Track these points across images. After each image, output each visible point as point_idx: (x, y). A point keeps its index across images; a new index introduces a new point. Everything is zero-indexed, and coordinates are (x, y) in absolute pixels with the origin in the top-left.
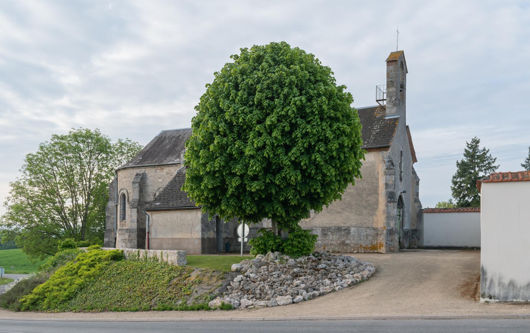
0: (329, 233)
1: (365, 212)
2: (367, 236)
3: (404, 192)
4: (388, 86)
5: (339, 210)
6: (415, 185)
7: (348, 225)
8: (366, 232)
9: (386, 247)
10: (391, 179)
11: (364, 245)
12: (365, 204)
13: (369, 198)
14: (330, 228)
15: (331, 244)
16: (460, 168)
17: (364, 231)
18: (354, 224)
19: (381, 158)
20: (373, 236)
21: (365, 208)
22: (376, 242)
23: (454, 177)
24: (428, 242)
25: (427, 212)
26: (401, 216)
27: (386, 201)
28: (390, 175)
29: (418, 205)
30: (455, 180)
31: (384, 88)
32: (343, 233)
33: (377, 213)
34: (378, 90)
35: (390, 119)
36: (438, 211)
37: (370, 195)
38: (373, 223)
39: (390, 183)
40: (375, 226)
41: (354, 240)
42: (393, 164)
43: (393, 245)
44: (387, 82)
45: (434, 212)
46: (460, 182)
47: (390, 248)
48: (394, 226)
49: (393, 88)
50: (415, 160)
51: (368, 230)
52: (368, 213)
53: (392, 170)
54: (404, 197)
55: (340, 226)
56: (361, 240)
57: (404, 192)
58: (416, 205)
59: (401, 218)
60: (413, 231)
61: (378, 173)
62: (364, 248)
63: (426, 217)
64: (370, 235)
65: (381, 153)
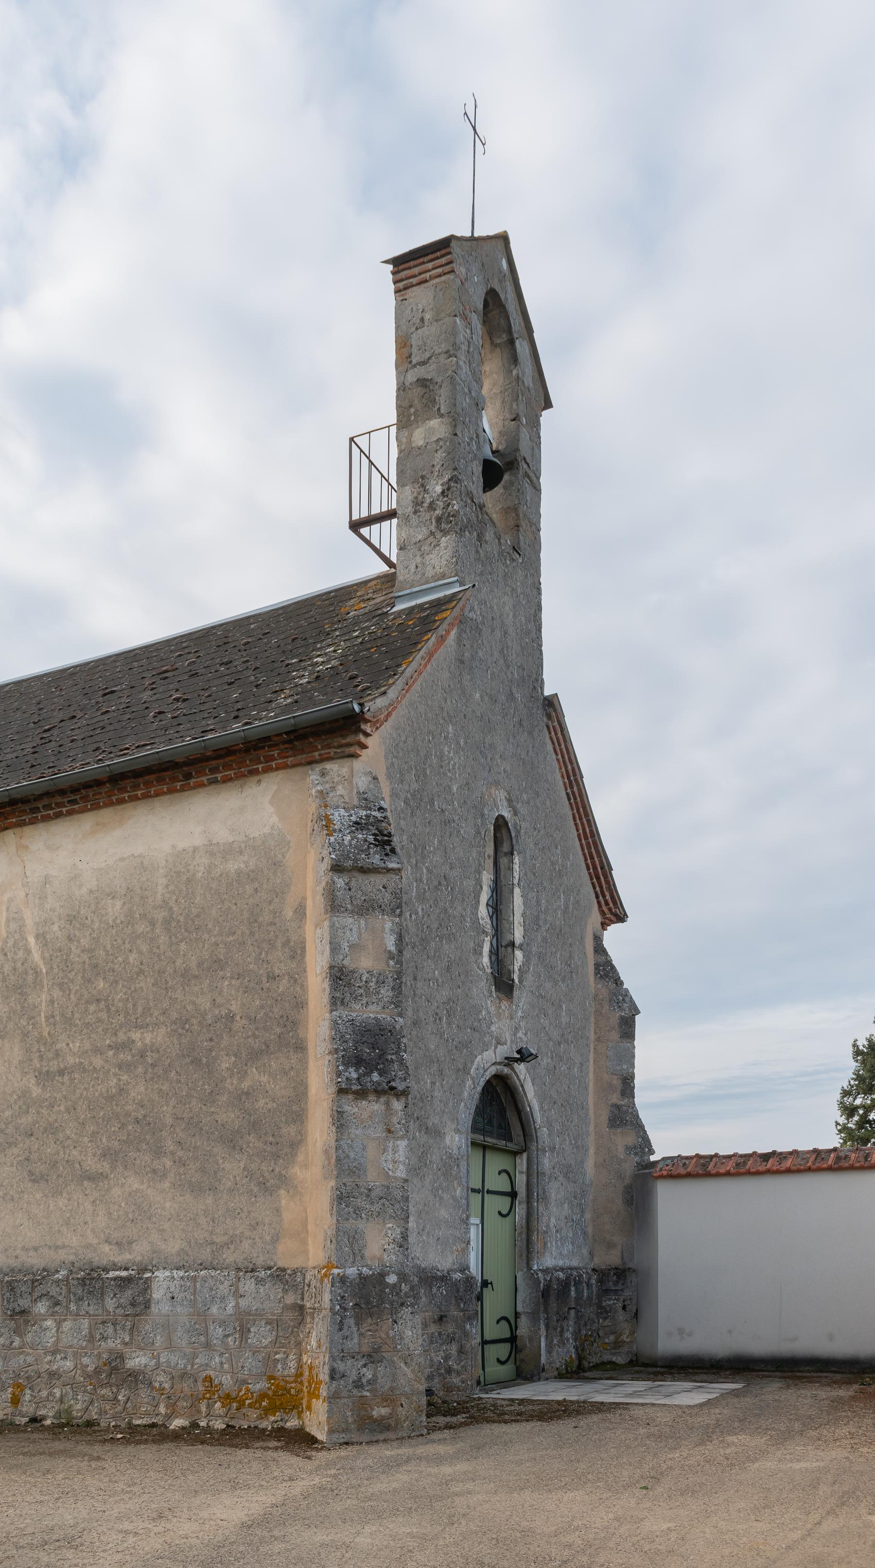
0: (41, 1308)
1: (232, 1167)
2: (243, 1324)
3: (524, 1056)
4: (407, 416)
5: (92, 1164)
6: (615, 1035)
7: (138, 1253)
8: (238, 1295)
9: (333, 1398)
10: (373, 943)
11: (227, 1381)
12: (230, 1117)
13: (255, 1076)
14: (48, 1272)
15: (53, 1375)
16: (863, 1062)
17: (224, 1289)
18: (173, 1247)
19: (313, 807)
20: (275, 1324)
21: (231, 1141)
22: (293, 1364)
23: (846, 1093)
24: (681, 1331)
25: (671, 1176)
26: (522, 1200)
27: (333, 1089)
28: (366, 908)
29: (631, 1139)
30: (848, 1100)
31: (385, 452)
32: (110, 1303)
33: (296, 1171)
34: (356, 451)
35: (411, 610)
36: (730, 1166)
37: (255, 1055)
38: (275, 1239)
39: (366, 963)
40: (286, 1256)
41: (170, 1347)
42: (384, 842)
43: (384, 1384)
44: (402, 389)
45: (708, 1175)
46: (863, 1106)
47: (362, 1404)
48: (391, 1258)
49: (434, 423)
50: (614, 912)
51: (248, 1285)
52: (249, 1174)
53: (378, 880)
54: (530, 1093)
55: (96, 1261)
56: (208, 1345)
57: (524, 1056)
58: (623, 1140)
59: (520, 1210)
60: (602, 1274)
61: (300, 911)
62: (227, 1398)
63: (670, 1201)
64: (259, 1314)
65: (313, 775)
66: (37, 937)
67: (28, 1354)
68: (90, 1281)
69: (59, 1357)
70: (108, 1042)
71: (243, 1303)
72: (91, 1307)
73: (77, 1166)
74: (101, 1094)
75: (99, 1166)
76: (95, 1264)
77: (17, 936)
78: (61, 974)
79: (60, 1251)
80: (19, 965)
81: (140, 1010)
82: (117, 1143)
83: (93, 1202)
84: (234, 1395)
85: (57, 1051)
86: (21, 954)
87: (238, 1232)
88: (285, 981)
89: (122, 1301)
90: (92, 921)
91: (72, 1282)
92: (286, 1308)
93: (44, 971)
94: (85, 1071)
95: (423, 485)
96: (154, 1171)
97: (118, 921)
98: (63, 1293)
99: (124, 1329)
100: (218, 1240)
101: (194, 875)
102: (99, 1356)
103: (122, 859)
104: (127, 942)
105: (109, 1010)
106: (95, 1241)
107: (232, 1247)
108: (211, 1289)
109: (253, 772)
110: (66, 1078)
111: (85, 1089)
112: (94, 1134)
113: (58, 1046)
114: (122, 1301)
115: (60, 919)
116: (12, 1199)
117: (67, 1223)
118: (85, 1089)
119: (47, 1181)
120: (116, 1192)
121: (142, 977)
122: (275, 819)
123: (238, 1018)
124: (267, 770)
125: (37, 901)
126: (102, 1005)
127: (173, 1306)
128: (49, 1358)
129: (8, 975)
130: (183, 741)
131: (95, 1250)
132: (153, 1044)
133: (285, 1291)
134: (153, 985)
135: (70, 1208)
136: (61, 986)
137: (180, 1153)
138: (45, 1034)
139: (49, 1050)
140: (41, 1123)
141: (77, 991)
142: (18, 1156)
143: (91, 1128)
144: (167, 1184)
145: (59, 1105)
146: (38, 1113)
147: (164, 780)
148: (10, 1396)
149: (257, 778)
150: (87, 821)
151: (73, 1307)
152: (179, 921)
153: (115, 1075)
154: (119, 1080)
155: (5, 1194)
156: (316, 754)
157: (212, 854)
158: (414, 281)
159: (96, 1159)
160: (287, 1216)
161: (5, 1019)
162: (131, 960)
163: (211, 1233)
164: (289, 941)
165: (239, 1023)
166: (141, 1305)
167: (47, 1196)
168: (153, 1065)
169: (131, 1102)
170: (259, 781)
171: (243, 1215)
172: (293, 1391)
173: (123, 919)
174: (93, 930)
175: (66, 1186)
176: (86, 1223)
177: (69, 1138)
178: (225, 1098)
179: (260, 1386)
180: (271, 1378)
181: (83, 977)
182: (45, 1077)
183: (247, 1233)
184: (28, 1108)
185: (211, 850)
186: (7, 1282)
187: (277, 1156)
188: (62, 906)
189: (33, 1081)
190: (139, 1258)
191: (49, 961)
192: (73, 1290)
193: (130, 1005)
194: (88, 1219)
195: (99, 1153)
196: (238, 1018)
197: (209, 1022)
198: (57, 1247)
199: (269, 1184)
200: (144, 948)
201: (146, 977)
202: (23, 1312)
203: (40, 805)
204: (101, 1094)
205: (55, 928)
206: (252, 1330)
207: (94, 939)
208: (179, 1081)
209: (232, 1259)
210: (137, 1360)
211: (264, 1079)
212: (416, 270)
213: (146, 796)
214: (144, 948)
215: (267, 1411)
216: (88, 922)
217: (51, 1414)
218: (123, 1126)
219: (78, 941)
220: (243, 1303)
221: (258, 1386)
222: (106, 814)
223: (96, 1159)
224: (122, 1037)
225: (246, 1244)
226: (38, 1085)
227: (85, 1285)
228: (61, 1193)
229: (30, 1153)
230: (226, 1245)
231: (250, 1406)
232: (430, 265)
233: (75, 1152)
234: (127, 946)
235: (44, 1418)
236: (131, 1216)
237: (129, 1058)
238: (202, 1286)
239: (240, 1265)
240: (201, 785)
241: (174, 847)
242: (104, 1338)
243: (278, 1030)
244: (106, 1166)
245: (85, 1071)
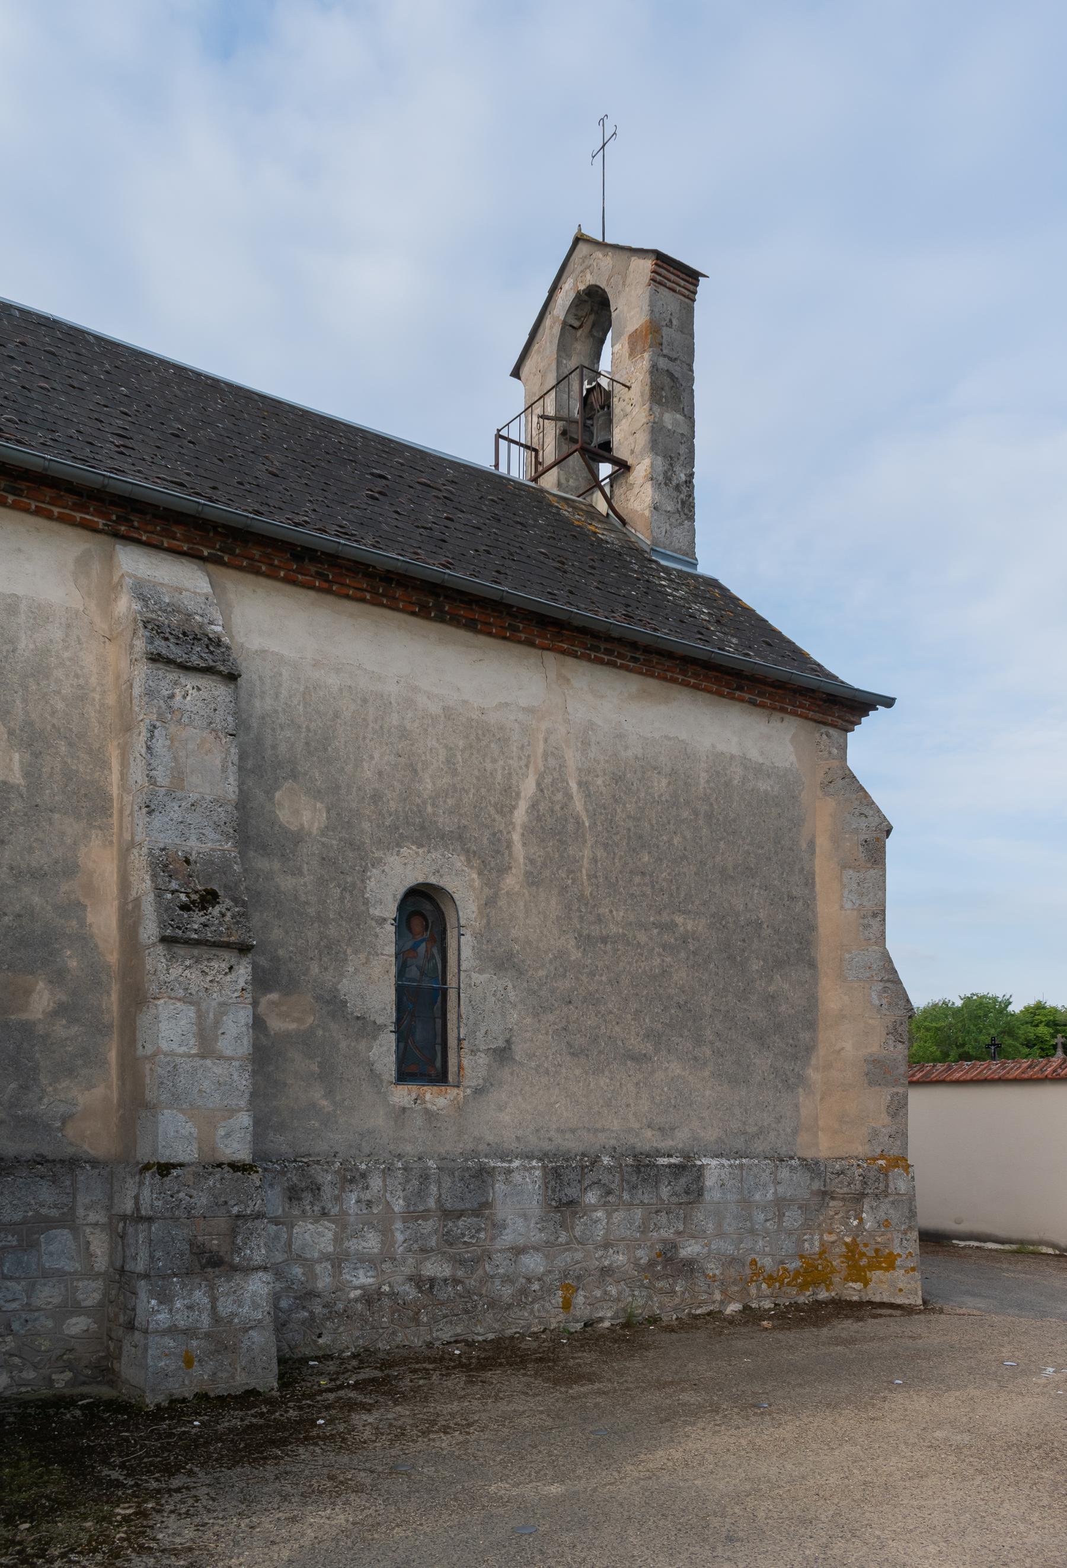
0: (591, 1197)
7: (681, 1138)
11: (767, 1262)
15: (606, 1272)
17: (766, 1177)
32: (665, 1191)
38: (795, 1132)
41: (720, 1235)
62: (770, 1279)
66: (580, 784)
67: (577, 1250)
68: (642, 1168)
69: (611, 1251)
70: (652, 919)
71: (780, 1189)
72: (646, 1196)
73: (620, 1043)
74: (645, 971)
75: (642, 1046)
76: (638, 1150)
77: (556, 775)
78: (605, 834)
79: (600, 1134)
80: (557, 807)
81: (682, 895)
82: (660, 1026)
83: (637, 1084)
84: (775, 1275)
85: (599, 915)
86: (559, 796)
87: (765, 1124)
88: (800, 903)
89: (677, 1188)
90: (638, 789)
91: (625, 1168)
92: (813, 1193)
93: (587, 824)
94: (629, 944)
95: (671, 465)
96: (695, 1059)
97: (663, 799)
98: (616, 1181)
99: (678, 1218)
100: (750, 1131)
101: (730, 780)
102: (652, 1246)
103: (667, 737)
104: (672, 822)
105: (653, 887)
106: (637, 1126)
107: (761, 1137)
108: (756, 1177)
109: (783, 710)
110: (609, 947)
111: (629, 963)
112: (637, 1012)
113: (601, 911)
114: (677, 1188)
115: (605, 774)
116: (547, 1072)
117: (608, 1104)
118: (629, 963)
119: (587, 1056)
120: (660, 1075)
121: (685, 863)
122: (793, 758)
123: (765, 926)
124: (794, 713)
125: (579, 744)
126: (647, 879)
127: (724, 1194)
128: (600, 1253)
129: (544, 815)
130: (228, 505)
131: (637, 1135)
132: (694, 932)
133: (812, 1179)
134: (696, 874)
135: (612, 1088)
136: (606, 846)
137: (718, 1044)
138: (587, 893)
139: (591, 913)
140: (580, 991)
141: (621, 858)
142: (554, 1024)
143: (634, 1006)
144: (707, 1073)
145: (601, 975)
146: (577, 979)
147: (699, 675)
148: (561, 1300)
149: (782, 715)
150: (634, 683)
151: (626, 1196)
152: (718, 820)
153: (659, 955)
154: (663, 961)
155: (538, 1066)
156: (830, 718)
157: (746, 768)
158: (669, 284)
159: (639, 1039)
160: (803, 1112)
161: (539, 864)
162: (675, 842)
163: (744, 1123)
164: (803, 869)
165: (766, 932)
166: (695, 1192)
167: (587, 1073)
168: (695, 953)
169: (673, 985)
170: (782, 720)
171: (770, 1108)
172: (820, 1267)
173: (668, 798)
174: (638, 797)
175: (608, 1064)
176: (628, 1105)
177: (611, 1012)
178: (755, 998)
179: (794, 1265)
180: (801, 1257)
181: (628, 844)
182: (586, 941)
183: (774, 1125)
184: (566, 971)
185: (745, 762)
186: (553, 1168)
187: (795, 1058)
188: (607, 761)
189: (573, 942)
190: (680, 1146)
191: (593, 816)
192: (626, 1177)
193: (674, 887)
194: (631, 1101)
195: (642, 1033)
196: (765, 926)
197: (742, 923)
198: (597, 1130)
199: (790, 1082)
200: (689, 835)
201: (689, 864)
202: (571, 1203)
203: (602, 647)
204: (645, 971)
205: (599, 782)
206: (787, 1214)
207: (640, 808)
208: (717, 974)
209: (761, 1149)
210: (689, 1249)
211: (786, 986)
212: (673, 277)
213: (696, 687)
214: (689, 835)
215: (803, 1287)
216: (634, 788)
217: (609, 1315)
218: (666, 1009)
219: (624, 805)
220: (780, 1189)
221: (794, 1265)
222: (653, 684)
223: (639, 1039)
224: (665, 917)
225: (772, 1135)
226: (578, 948)
227: (640, 1172)
228: (603, 1072)
229: (569, 1022)
230: (756, 1135)
231: (788, 1284)
232: (682, 283)
233: (617, 1028)
234: (672, 827)
235: (601, 1320)
236: (673, 1102)
237: (672, 940)
238: (748, 1174)
239: (767, 1155)
240: (741, 700)
241: (713, 746)
242: (657, 1227)
243: (796, 946)
244: (649, 1048)
245: (629, 944)
